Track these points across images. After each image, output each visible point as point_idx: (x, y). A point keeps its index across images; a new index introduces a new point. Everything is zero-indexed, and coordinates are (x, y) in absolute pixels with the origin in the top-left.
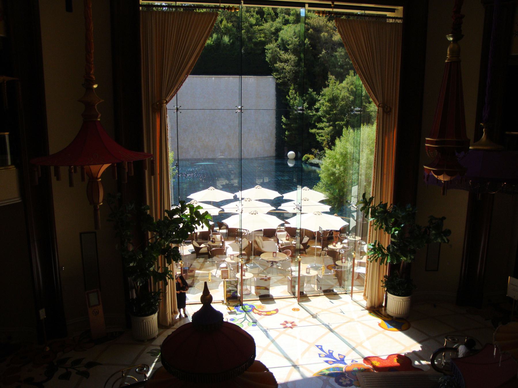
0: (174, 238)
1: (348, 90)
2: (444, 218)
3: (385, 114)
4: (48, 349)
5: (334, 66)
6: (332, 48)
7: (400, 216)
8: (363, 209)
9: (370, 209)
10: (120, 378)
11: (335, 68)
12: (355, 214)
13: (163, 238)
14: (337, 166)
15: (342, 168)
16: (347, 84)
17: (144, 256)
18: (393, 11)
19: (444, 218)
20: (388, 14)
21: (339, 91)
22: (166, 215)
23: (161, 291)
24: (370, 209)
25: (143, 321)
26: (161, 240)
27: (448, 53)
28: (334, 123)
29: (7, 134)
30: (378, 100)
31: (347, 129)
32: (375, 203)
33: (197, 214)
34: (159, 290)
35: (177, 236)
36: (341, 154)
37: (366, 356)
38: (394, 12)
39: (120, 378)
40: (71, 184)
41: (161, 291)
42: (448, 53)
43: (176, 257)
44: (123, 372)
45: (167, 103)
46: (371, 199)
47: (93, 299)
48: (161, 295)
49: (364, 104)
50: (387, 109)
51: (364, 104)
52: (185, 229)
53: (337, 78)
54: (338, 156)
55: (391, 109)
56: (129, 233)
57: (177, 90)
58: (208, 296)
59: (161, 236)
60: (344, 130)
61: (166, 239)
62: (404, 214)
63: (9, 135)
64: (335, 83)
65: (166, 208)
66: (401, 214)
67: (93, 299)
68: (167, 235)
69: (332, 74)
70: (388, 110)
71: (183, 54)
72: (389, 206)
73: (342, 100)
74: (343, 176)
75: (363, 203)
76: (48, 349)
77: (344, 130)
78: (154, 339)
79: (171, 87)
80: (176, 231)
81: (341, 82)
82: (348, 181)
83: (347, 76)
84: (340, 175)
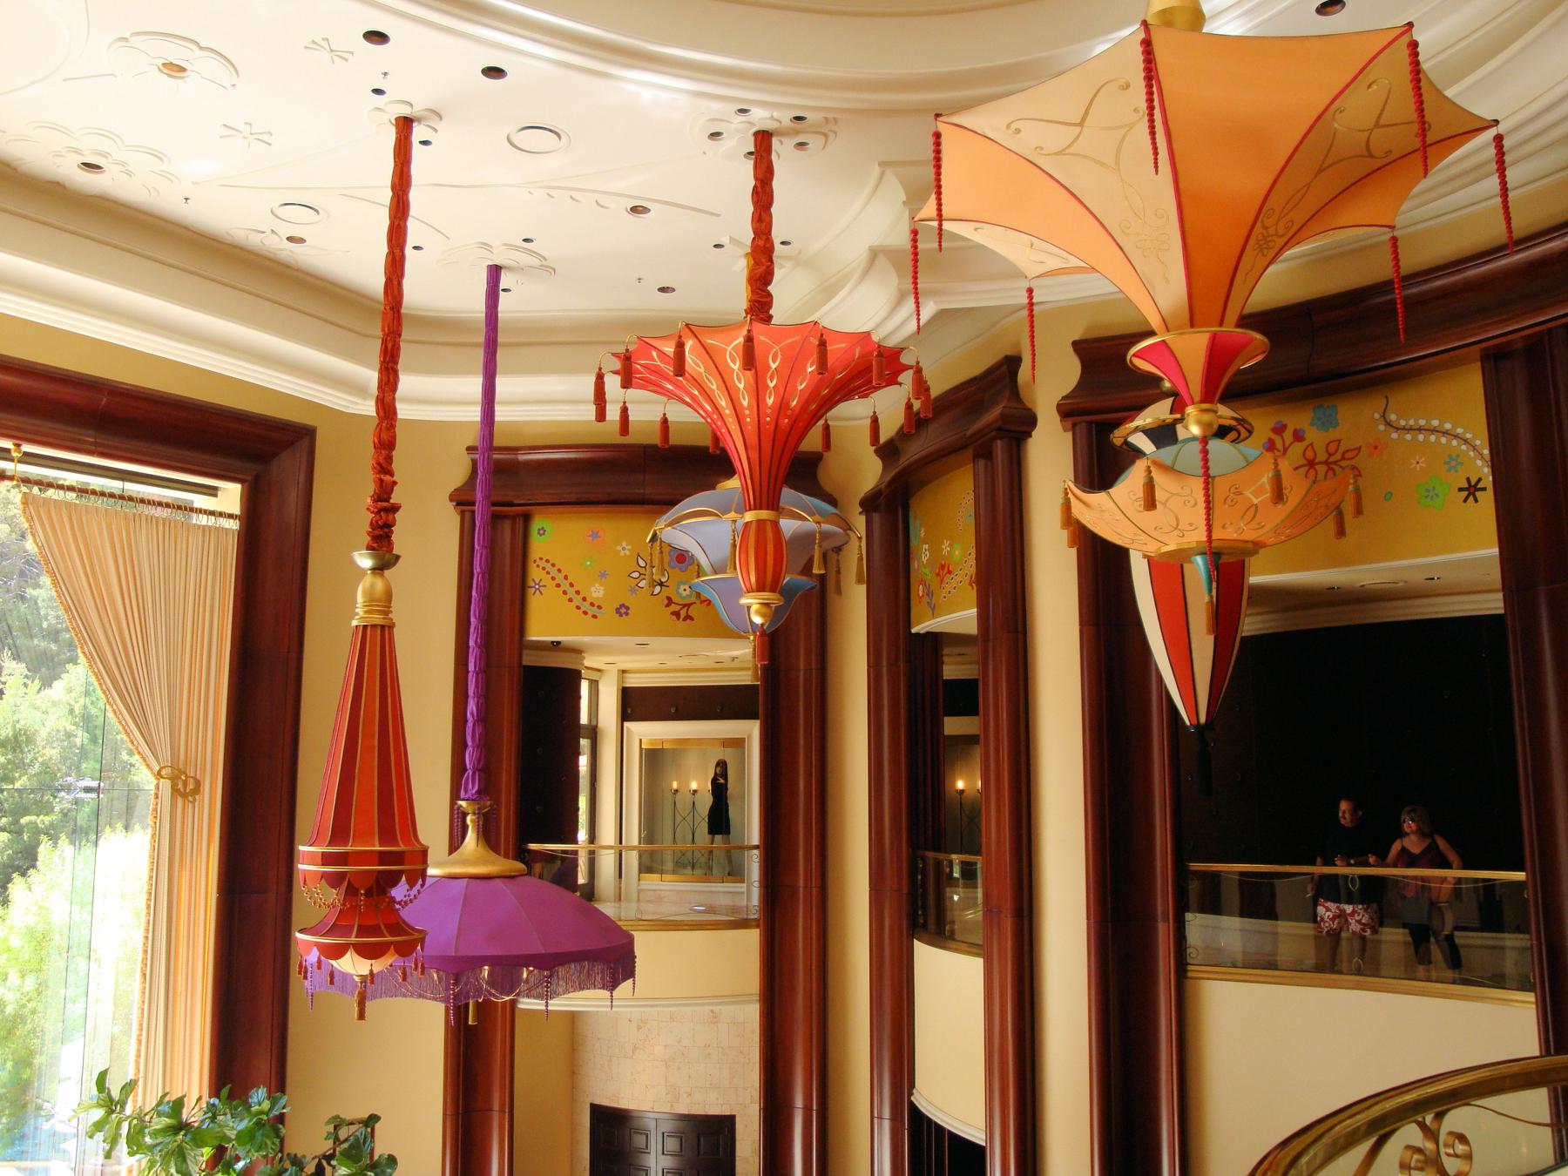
1: (71, 711)
2: (373, 1119)
3: (180, 800)
5: (28, 629)
6: (22, 574)
7: (232, 1134)
8: (99, 1126)
9: (125, 1126)
11: (31, 637)
12: (70, 1146)
14: (14, 977)
15: (30, 983)
16: (70, 691)
18: (212, 491)
19: (373, 1119)
20: (200, 501)
21: (38, 715)
24: (125, 1126)
27: (360, 599)
28: (16, 822)
30: (156, 756)
31: (55, 845)
32: (144, 1100)
36: (31, 933)
38: (215, 496)
42: (360, 599)
46: (129, 1087)
49: (124, 756)
50: (185, 783)
51: (124, 756)
53: (33, 669)
54: (15, 941)
55: (198, 783)
60: (44, 849)
62: (244, 1124)
64: (26, 685)
66: (233, 1126)
69: (17, 657)
70: (191, 786)
72: (190, 1102)
73: (49, 742)
74: (34, 1012)
75: (99, 1105)
77: (41, 849)
81: (47, 683)
82: (50, 1023)
83: (69, 666)
84: (24, 1006)
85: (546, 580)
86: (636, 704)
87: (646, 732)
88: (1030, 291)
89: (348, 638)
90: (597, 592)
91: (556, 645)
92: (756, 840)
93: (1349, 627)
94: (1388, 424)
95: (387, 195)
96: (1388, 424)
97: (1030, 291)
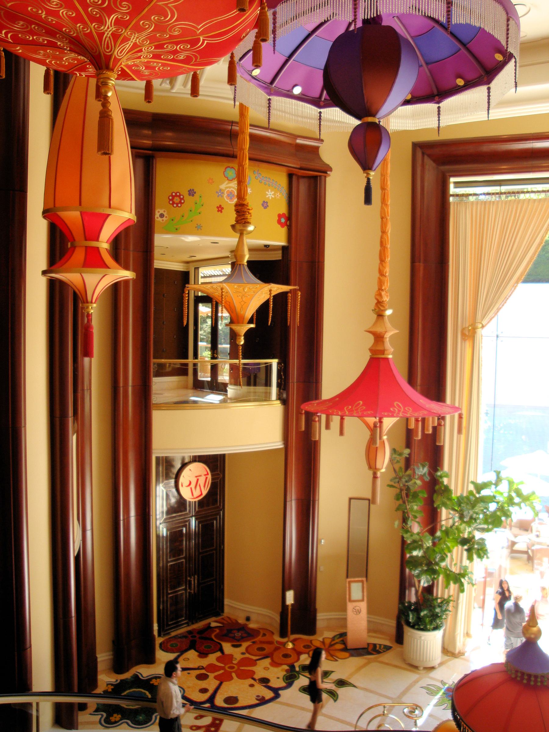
0: (480, 524)
4: (290, 646)
10: (379, 715)
13: (464, 522)
17: (434, 544)
22: (471, 487)
23: (451, 598)
25: (420, 637)
26: (461, 524)
29: (274, 362)
33: (519, 493)
34: (449, 596)
35: (486, 521)
37: (481, 610)
39: (379, 715)
40: (341, 433)
41: (451, 598)
43: (481, 552)
44: (384, 707)
45: (483, 327)
47: (356, 590)
48: (451, 604)
52: (498, 513)
56: (415, 508)
57: (499, 309)
58: (535, 629)
59: (462, 517)
61: (469, 523)
63: (278, 364)
65: (472, 478)
67: (356, 590)
68: (471, 518)
71: (508, 263)
76: (290, 646)
78: (433, 668)
79: (486, 314)
80: (484, 513)
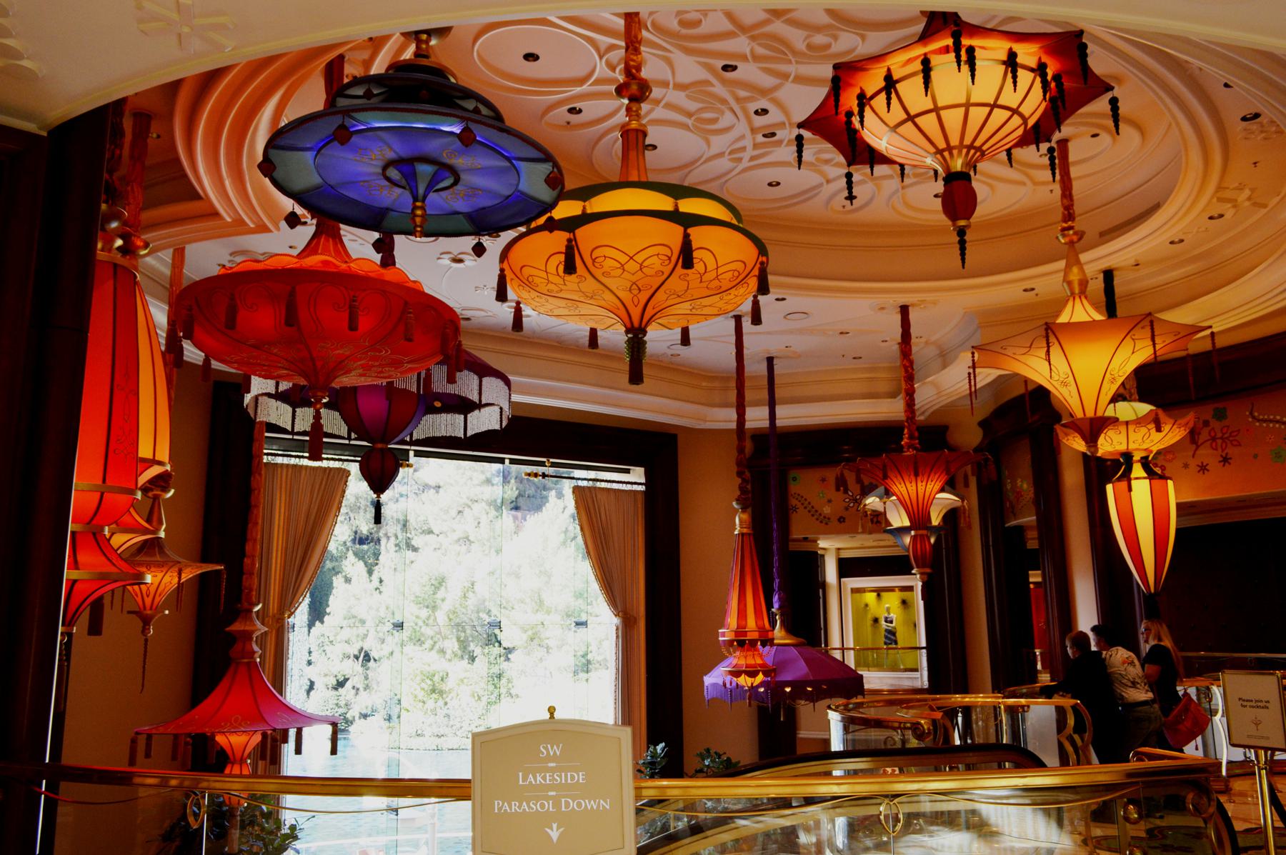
18: (627, 471)
85: (799, 504)
86: (848, 567)
87: (852, 582)
88: (904, 310)
89: (735, 544)
90: (827, 510)
91: (806, 539)
92: (924, 644)
93: (85, 341)
94: (1254, 417)
95: (733, 339)
96: (1254, 417)
97: (904, 310)
